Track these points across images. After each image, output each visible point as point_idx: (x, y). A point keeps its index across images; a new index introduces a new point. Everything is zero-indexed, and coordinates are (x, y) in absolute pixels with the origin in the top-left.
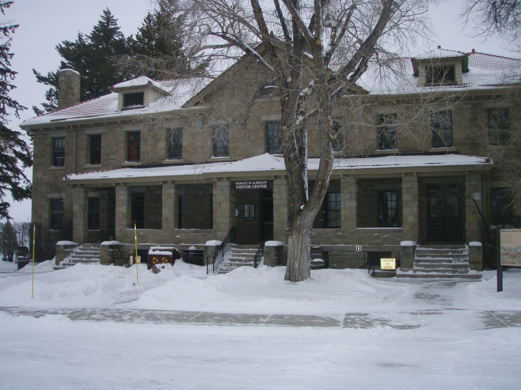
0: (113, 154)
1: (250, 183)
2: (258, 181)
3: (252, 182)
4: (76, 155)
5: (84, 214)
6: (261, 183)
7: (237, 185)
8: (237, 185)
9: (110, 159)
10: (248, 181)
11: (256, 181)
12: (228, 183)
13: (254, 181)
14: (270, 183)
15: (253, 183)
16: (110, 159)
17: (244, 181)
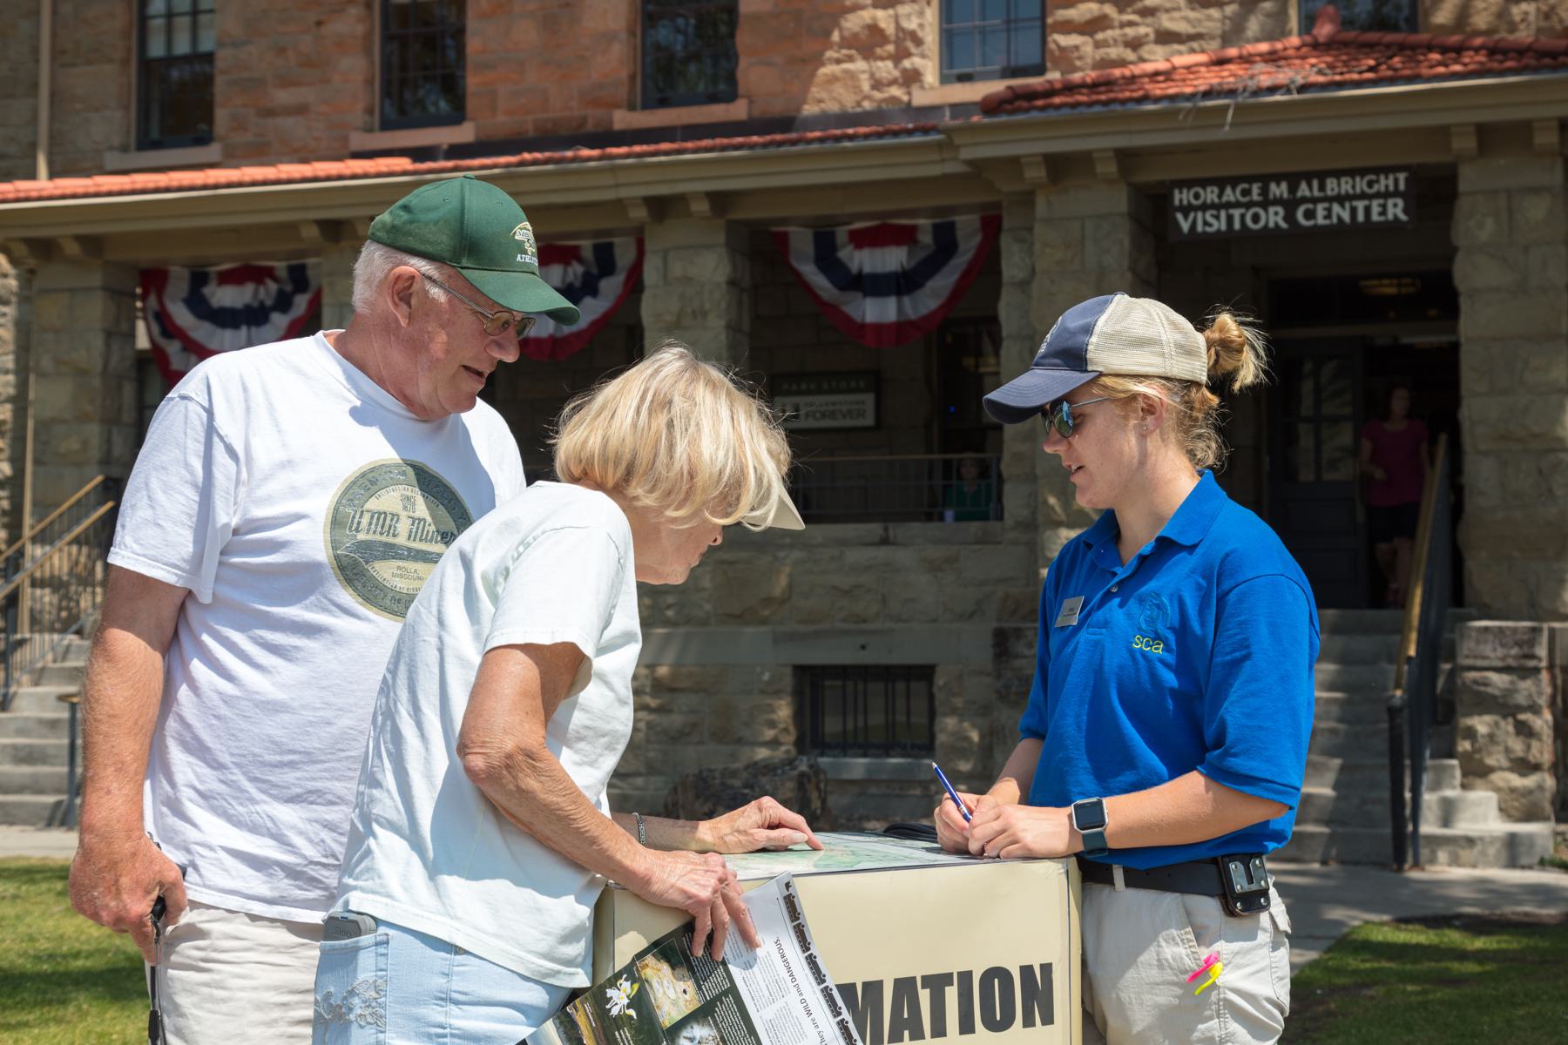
0: (286, 82)
1: (1279, 190)
2: (1338, 174)
3: (1293, 180)
4: (53, 95)
5: (109, 441)
6: (1361, 184)
7: (1187, 210)
8: (1187, 210)
9: (270, 113)
10: (1265, 180)
11: (1322, 176)
12: (1118, 201)
13: (1308, 176)
14: (1434, 192)
15: (1303, 190)
16: (270, 113)
17: (1234, 181)
